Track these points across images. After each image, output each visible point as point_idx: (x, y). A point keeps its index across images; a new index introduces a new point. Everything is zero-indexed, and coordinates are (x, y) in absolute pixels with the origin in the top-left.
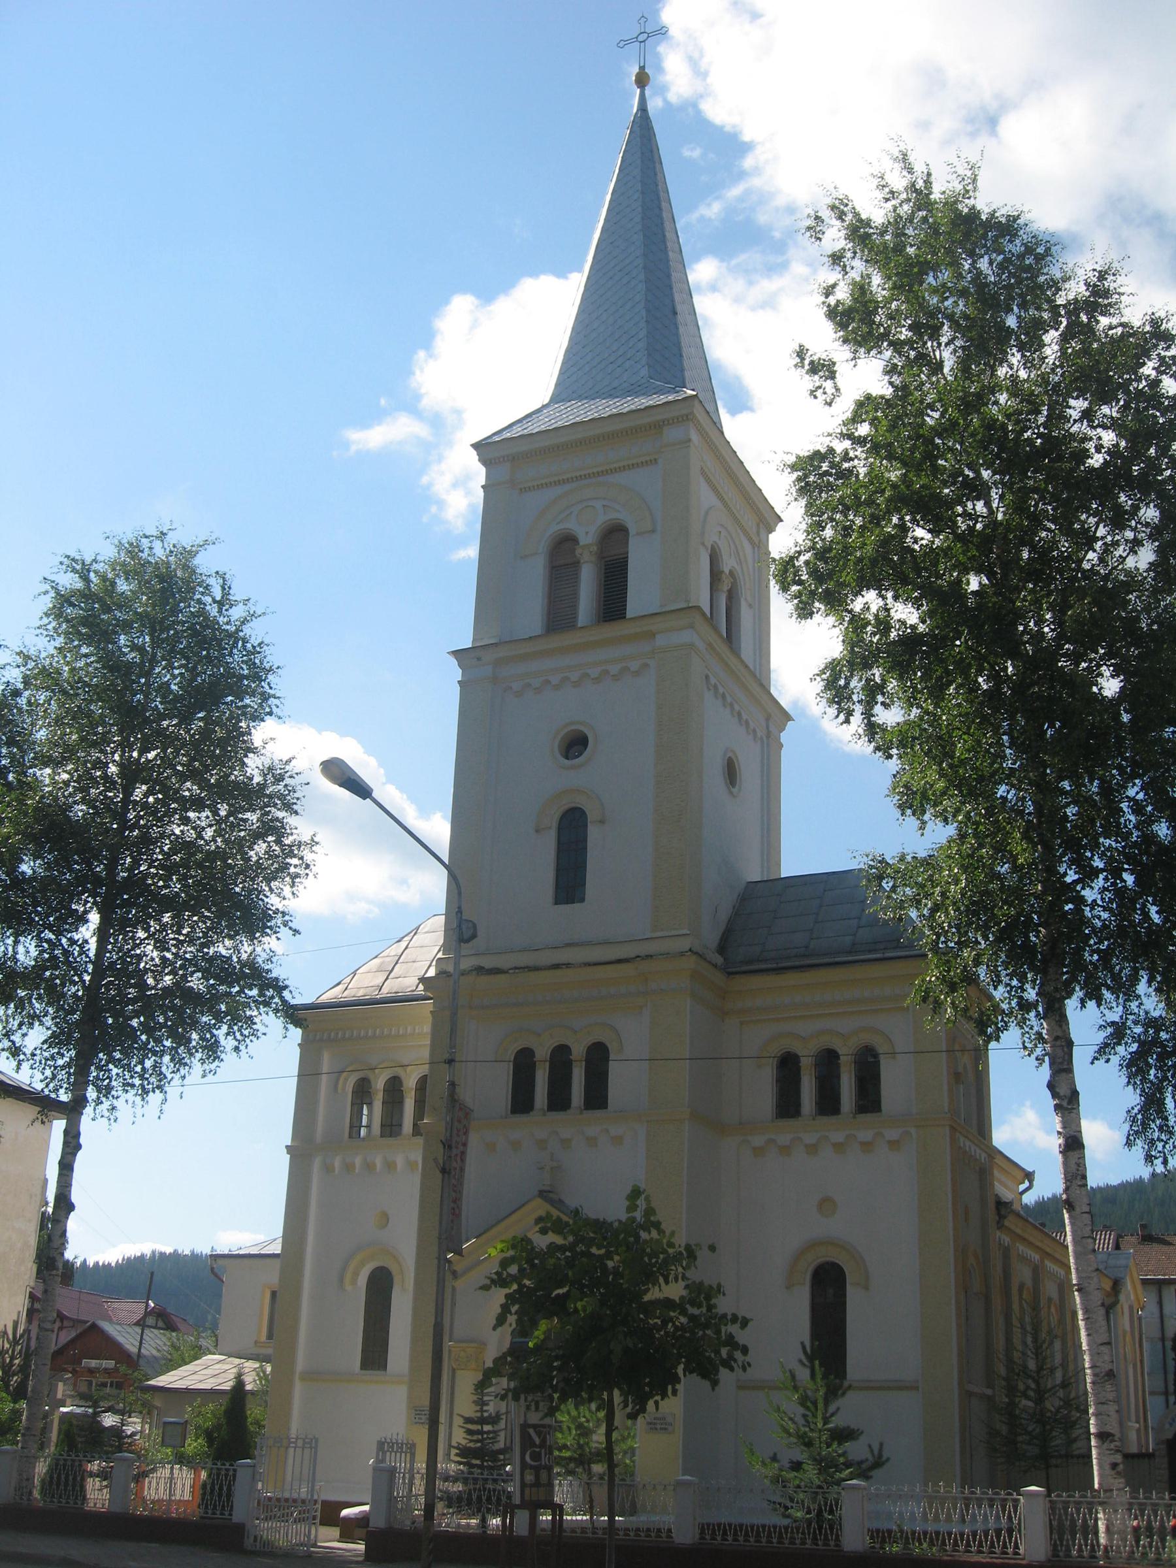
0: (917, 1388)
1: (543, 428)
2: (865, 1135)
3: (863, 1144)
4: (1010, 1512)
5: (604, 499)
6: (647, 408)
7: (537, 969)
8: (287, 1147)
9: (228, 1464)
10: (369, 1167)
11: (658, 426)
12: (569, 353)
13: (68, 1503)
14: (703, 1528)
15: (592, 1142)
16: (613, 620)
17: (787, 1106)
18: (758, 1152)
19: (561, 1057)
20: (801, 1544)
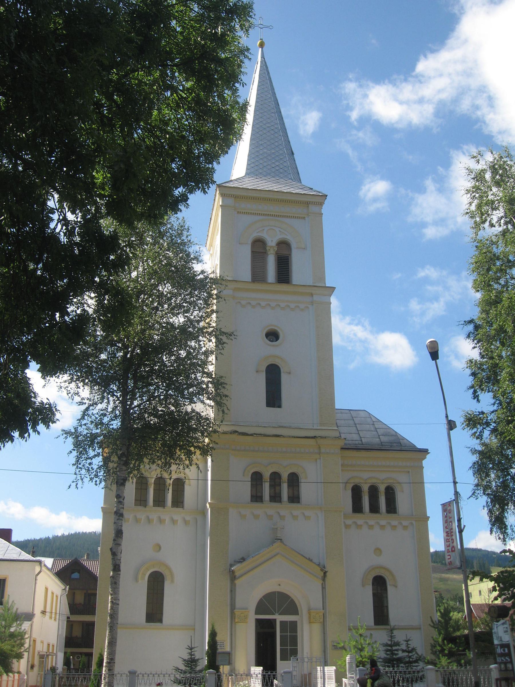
0: (420, 629)
1: (244, 186)
2: (371, 522)
3: (404, 526)
4: (267, 680)
5: (269, 226)
6: (304, 194)
8: (102, 507)
10: (149, 520)
11: (307, 204)
12: (249, 155)
16: (284, 283)
17: (357, 508)
18: (347, 526)
19: (275, 477)
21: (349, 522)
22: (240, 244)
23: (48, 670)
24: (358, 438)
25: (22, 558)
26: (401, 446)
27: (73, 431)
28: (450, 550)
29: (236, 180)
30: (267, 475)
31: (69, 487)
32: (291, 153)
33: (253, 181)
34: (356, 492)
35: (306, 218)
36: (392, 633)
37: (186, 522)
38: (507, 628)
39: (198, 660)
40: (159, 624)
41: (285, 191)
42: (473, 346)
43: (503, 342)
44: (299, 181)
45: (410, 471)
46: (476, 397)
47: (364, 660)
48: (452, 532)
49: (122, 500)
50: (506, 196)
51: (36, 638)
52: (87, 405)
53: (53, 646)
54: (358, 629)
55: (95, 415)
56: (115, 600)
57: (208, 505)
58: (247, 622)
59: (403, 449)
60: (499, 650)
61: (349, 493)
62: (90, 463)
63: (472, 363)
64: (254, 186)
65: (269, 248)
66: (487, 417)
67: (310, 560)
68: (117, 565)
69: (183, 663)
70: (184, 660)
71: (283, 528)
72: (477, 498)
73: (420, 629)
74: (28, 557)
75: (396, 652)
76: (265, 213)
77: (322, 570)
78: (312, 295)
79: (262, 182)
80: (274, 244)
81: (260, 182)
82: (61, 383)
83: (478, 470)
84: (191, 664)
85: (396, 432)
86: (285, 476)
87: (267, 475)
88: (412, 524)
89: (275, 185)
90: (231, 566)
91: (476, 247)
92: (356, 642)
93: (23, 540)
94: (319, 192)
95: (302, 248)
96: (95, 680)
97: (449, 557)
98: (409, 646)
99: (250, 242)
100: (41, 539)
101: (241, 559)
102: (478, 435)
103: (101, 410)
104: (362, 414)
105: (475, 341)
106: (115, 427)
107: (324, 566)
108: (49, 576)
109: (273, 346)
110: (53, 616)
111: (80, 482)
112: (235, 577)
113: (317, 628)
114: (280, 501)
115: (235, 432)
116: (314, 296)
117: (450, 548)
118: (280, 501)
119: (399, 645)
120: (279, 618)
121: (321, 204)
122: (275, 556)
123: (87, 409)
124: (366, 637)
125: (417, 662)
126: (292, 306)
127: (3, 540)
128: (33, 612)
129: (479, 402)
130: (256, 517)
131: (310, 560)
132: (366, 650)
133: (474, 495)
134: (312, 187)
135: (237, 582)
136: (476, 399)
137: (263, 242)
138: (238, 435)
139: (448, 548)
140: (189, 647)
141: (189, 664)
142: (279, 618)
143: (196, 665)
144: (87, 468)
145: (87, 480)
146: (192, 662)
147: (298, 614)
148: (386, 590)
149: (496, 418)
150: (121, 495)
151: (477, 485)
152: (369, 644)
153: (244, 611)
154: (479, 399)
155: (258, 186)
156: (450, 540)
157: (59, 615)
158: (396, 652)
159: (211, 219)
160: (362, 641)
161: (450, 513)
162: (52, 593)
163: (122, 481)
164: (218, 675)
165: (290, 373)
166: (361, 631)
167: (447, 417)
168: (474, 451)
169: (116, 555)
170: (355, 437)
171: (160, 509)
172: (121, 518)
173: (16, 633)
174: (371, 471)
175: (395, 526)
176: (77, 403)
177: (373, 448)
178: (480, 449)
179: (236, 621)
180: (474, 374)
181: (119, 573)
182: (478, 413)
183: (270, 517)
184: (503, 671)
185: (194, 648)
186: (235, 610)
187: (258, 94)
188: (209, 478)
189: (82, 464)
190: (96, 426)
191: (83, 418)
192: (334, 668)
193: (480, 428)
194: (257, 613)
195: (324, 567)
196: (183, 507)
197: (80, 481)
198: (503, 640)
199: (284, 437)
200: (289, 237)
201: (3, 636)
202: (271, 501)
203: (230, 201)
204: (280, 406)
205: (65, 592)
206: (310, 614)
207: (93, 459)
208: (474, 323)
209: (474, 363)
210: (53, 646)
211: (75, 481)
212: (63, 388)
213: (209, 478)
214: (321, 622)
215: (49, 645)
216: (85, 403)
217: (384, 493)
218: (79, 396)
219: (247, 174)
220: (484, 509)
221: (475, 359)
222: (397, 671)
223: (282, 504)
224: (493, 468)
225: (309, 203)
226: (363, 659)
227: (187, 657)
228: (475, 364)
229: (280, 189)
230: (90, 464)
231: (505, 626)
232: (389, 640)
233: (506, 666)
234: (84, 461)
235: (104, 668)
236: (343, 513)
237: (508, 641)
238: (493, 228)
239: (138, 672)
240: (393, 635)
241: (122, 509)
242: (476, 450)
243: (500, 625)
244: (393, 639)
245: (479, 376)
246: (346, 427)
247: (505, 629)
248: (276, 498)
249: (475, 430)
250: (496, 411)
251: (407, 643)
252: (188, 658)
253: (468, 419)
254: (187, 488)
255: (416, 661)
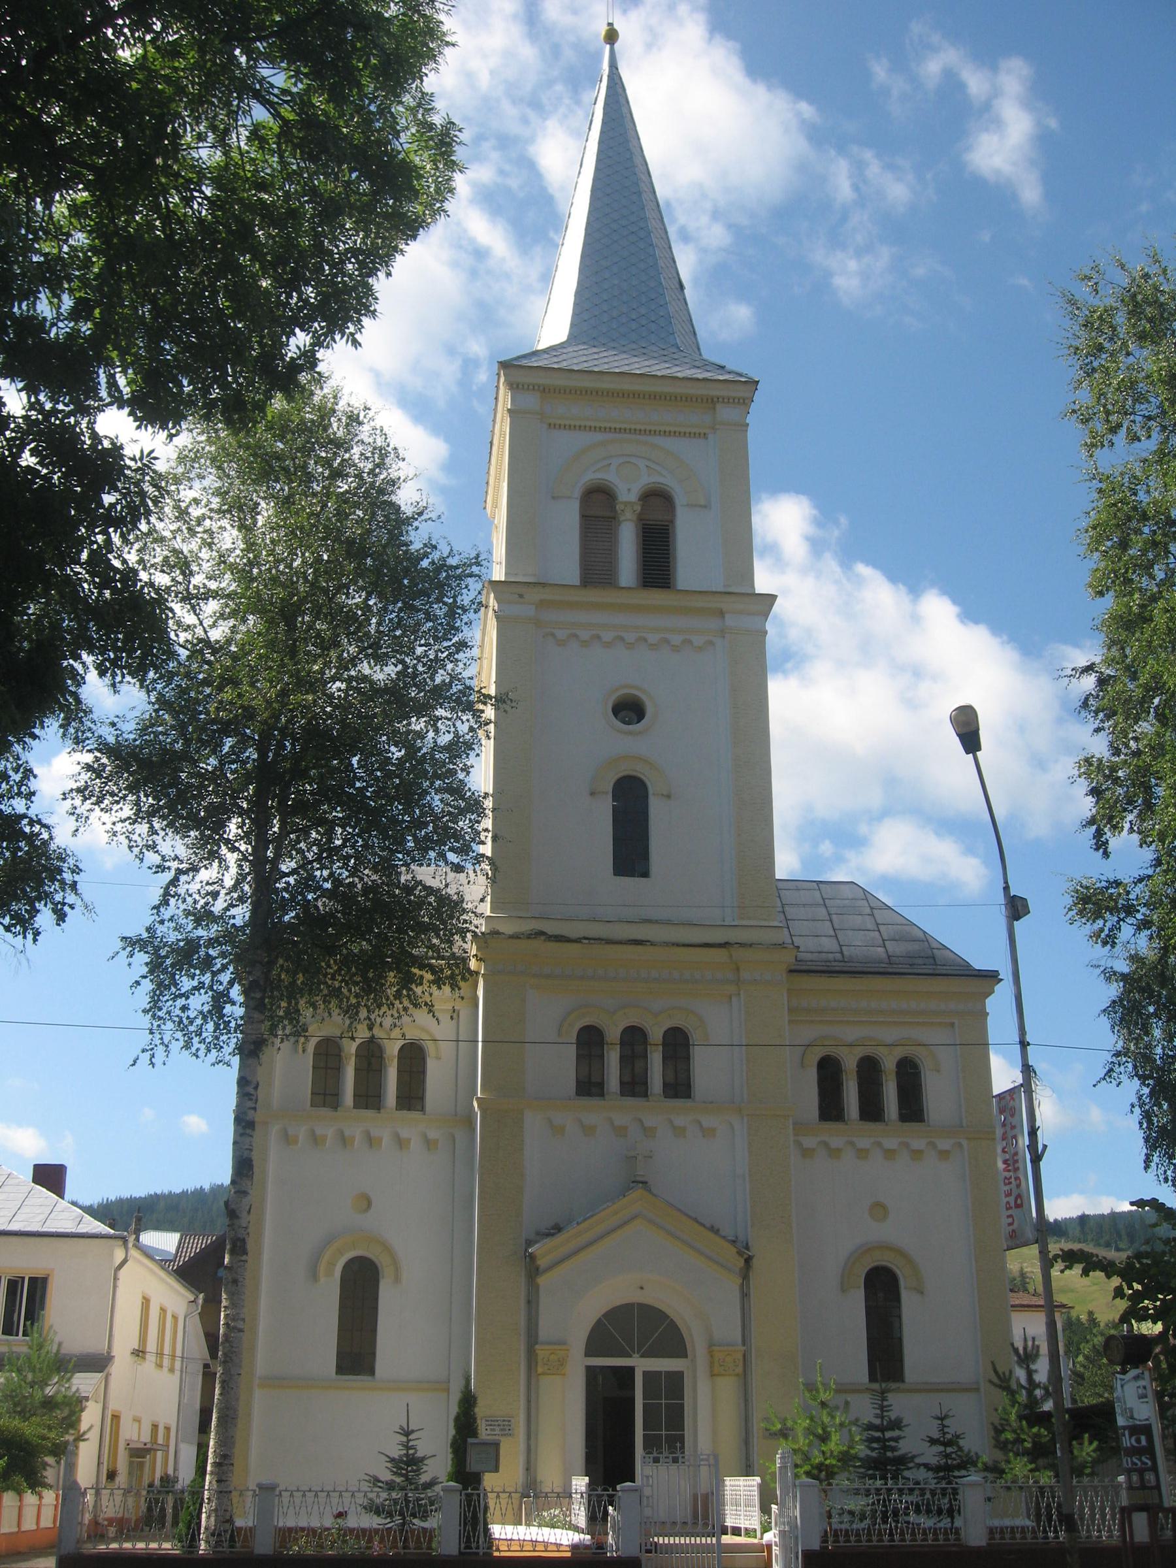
0: (977, 1390)
1: (564, 365)
2: (863, 1143)
5: (649, 460)
6: (705, 380)
7: (610, 942)
9: (599, 1489)
10: (344, 1140)
11: (712, 402)
12: (578, 294)
13: (849, 1541)
14: (991, 1531)
15: (679, 1132)
16: (659, 587)
17: (830, 1109)
18: (806, 1153)
19: (634, 1038)
20: (878, 1541)
21: (809, 1142)
22: (553, 498)
23: (151, 1485)
24: (836, 948)
25: (84, 1231)
26: (936, 965)
27: (145, 935)
28: (1012, 1204)
29: (545, 351)
30: (613, 1033)
31: (135, 1062)
32: (678, 286)
33: (585, 352)
34: (829, 1071)
35: (711, 437)
36: (884, 1399)
37: (429, 1144)
38: (1145, 1387)
39: (423, 1459)
40: (370, 1378)
41: (659, 374)
42: (1096, 726)
43: (1163, 715)
44: (696, 350)
45: (956, 1021)
46: (1101, 845)
47: (828, 1462)
48: (1017, 1161)
49: (252, 1091)
50: (1161, 370)
51: (120, 1412)
52: (173, 872)
53: (168, 1429)
54: (818, 1391)
55: (194, 896)
56: (234, 1320)
57: (475, 1104)
58: (564, 1375)
59: (937, 972)
60: (1127, 1441)
61: (812, 1075)
62: (184, 1006)
63: (1091, 765)
64: (586, 365)
65: (622, 507)
66: (1128, 893)
67: (715, 1230)
68: (239, 1239)
69: (389, 1465)
70: (392, 1460)
71: (651, 1157)
72: (1119, 1083)
73: (977, 1390)
74: (89, 1223)
75: (892, 1444)
76: (588, 424)
77: (740, 1253)
78: (721, 614)
79: (605, 354)
80: (633, 497)
81: (602, 355)
82: (114, 824)
83: (1122, 1019)
84: (406, 1470)
85: (925, 932)
86: (656, 1034)
87: (613, 1033)
88: (960, 1145)
89: (636, 359)
90: (529, 1243)
91: (1100, 491)
92: (812, 1419)
93: (143, 1196)
94: (741, 375)
95: (701, 506)
96: (194, 1504)
97: (1010, 1220)
98: (946, 1430)
99: (577, 493)
100: (184, 1194)
101: (553, 1229)
102: (1107, 936)
103: (208, 883)
104: (846, 892)
105: (1101, 715)
106: (239, 922)
107: (747, 1244)
108: (151, 1270)
109: (630, 733)
110: (166, 1362)
111: (160, 1051)
112: (537, 1269)
113: (728, 1386)
114: (645, 1094)
115: (542, 933)
116: (727, 616)
117: (1011, 1199)
118: (645, 1094)
119: (900, 1429)
120: (642, 1365)
121: (745, 403)
122: (633, 1218)
123: (174, 882)
124: (837, 1408)
125: (965, 1468)
126: (676, 639)
127: (44, 1190)
128: (109, 1353)
129: (1108, 857)
130: (589, 1130)
131: (715, 1230)
132: (835, 1438)
133: (1110, 1077)
134: (723, 364)
135: (542, 1280)
136: (1101, 850)
137: (608, 494)
138: (545, 941)
139: (1007, 1199)
140: (402, 1429)
141: (403, 1469)
142: (642, 1365)
143: (418, 1470)
144: (177, 1019)
145: (176, 1046)
146: (409, 1464)
147: (686, 1356)
148: (898, 1299)
149: (1148, 894)
150: (249, 1078)
151: (1125, 1052)
152: (842, 1425)
153: (556, 1347)
154: (1109, 850)
155: (596, 362)
156: (1013, 1180)
157: (182, 1361)
158: (892, 1444)
159: (491, 443)
160: (826, 1419)
161: (1012, 1115)
162: (162, 1309)
163: (252, 1047)
164: (467, 1495)
165: (669, 796)
166: (824, 1396)
167: (1006, 888)
168: (1110, 975)
169: (238, 1217)
170: (829, 944)
171: (370, 1113)
172: (248, 1131)
173: (59, 1398)
174: (895, 1023)
175: (893, 1152)
176: (149, 868)
177: (869, 970)
178: (1126, 970)
179: (540, 1370)
180: (1095, 792)
181: (244, 1258)
182: (1104, 884)
183: (621, 1131)
184: (1137, 1488)
185: (413, 1431)
186: (537, 1347)
187: (600, 152)
188: (480, 1039)
189: (165, 1010)
190: (198, 922)
191: (165, 902)
192: (758, 1479)
193: (1112, 920)
194: (589, 1353)
195: (747, 1248)
196: (423, 1109)
197: (161, 1048)
198: (1136, 1416)
199: (652, 944)
200: (669, 481)
201: (29, 1406)
202: (622, 1094)
203: (532, 401)
204: (645, 874)
205: (195, 1308)
206: (712, 1356)
207: (191, 997)
208: (1097, 672)
209: (1095, 764)
210: (168, 1429)
211: (149, 1050)
212: (118, 834)
213: (480, 1039)
214: (737, 1375)
215: (155, 1427)
216: (169, 868)
217: (855, 1074)
218: (157, 852)
219: (573, 337)
220: (1132, 1112)
221: (1098, 756)
222: (892, 1489)
223: (648, 1101)
224: (1156, 1015)
225: (715, 399)
226: (825, 1459)
227: (396, 1452)
228: (1098, 767)
229: (648, 369)
230: (184, 1008)
231: (1141, 1383)
232: (877, 1416)
233: (1142, 1479)
234: (170, 1003)
235: (208, 1477)
236: (791, 1121)
237: (1147, 1420)
238: (1137, 444)
239: (282, 1487)
240: (885, 1403)
241: (253, 1112)
242: (1115, 973)
243: (1129, 1381)
244: (885, 1414)
245: (1108, 794)
246: (805, 922)
247: (1140, 1391)
248: (634, 1086)
249: (1100, 922)
250: (1149, 877)
251: (942, 1424)
252: (400, 1456)
253: (1082, 899)
254: (431, 1065)
255: (962, 1466)
